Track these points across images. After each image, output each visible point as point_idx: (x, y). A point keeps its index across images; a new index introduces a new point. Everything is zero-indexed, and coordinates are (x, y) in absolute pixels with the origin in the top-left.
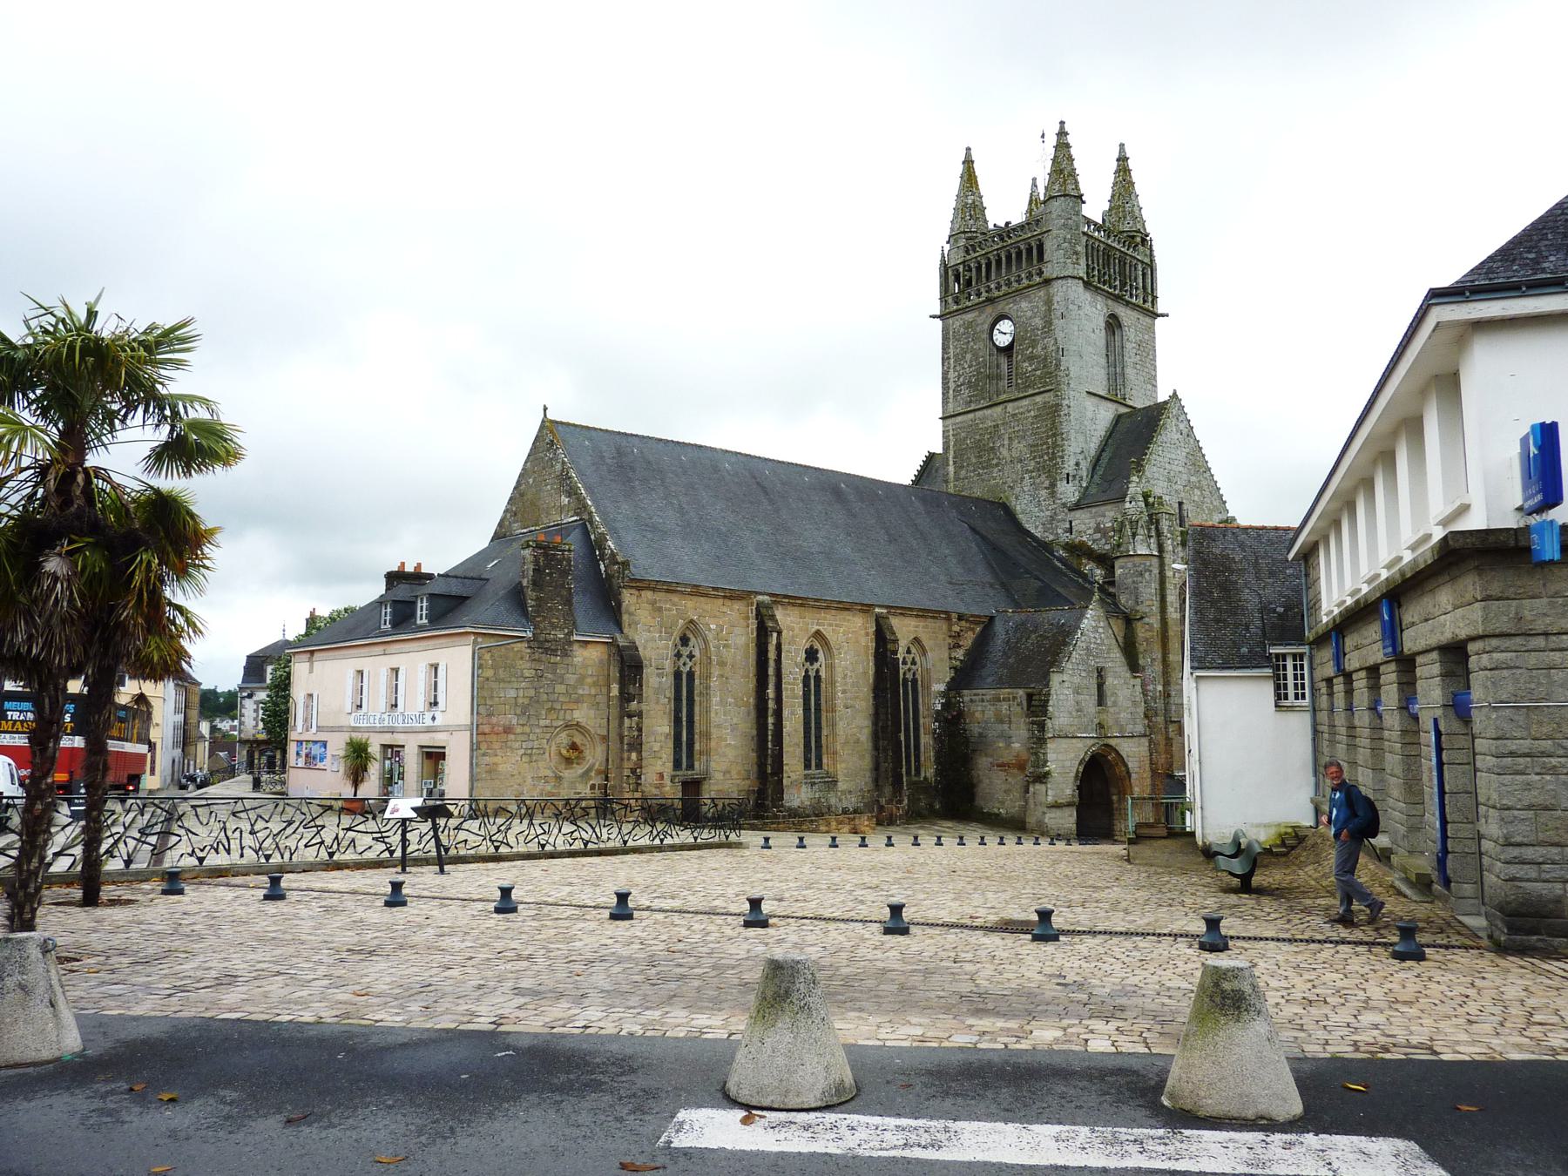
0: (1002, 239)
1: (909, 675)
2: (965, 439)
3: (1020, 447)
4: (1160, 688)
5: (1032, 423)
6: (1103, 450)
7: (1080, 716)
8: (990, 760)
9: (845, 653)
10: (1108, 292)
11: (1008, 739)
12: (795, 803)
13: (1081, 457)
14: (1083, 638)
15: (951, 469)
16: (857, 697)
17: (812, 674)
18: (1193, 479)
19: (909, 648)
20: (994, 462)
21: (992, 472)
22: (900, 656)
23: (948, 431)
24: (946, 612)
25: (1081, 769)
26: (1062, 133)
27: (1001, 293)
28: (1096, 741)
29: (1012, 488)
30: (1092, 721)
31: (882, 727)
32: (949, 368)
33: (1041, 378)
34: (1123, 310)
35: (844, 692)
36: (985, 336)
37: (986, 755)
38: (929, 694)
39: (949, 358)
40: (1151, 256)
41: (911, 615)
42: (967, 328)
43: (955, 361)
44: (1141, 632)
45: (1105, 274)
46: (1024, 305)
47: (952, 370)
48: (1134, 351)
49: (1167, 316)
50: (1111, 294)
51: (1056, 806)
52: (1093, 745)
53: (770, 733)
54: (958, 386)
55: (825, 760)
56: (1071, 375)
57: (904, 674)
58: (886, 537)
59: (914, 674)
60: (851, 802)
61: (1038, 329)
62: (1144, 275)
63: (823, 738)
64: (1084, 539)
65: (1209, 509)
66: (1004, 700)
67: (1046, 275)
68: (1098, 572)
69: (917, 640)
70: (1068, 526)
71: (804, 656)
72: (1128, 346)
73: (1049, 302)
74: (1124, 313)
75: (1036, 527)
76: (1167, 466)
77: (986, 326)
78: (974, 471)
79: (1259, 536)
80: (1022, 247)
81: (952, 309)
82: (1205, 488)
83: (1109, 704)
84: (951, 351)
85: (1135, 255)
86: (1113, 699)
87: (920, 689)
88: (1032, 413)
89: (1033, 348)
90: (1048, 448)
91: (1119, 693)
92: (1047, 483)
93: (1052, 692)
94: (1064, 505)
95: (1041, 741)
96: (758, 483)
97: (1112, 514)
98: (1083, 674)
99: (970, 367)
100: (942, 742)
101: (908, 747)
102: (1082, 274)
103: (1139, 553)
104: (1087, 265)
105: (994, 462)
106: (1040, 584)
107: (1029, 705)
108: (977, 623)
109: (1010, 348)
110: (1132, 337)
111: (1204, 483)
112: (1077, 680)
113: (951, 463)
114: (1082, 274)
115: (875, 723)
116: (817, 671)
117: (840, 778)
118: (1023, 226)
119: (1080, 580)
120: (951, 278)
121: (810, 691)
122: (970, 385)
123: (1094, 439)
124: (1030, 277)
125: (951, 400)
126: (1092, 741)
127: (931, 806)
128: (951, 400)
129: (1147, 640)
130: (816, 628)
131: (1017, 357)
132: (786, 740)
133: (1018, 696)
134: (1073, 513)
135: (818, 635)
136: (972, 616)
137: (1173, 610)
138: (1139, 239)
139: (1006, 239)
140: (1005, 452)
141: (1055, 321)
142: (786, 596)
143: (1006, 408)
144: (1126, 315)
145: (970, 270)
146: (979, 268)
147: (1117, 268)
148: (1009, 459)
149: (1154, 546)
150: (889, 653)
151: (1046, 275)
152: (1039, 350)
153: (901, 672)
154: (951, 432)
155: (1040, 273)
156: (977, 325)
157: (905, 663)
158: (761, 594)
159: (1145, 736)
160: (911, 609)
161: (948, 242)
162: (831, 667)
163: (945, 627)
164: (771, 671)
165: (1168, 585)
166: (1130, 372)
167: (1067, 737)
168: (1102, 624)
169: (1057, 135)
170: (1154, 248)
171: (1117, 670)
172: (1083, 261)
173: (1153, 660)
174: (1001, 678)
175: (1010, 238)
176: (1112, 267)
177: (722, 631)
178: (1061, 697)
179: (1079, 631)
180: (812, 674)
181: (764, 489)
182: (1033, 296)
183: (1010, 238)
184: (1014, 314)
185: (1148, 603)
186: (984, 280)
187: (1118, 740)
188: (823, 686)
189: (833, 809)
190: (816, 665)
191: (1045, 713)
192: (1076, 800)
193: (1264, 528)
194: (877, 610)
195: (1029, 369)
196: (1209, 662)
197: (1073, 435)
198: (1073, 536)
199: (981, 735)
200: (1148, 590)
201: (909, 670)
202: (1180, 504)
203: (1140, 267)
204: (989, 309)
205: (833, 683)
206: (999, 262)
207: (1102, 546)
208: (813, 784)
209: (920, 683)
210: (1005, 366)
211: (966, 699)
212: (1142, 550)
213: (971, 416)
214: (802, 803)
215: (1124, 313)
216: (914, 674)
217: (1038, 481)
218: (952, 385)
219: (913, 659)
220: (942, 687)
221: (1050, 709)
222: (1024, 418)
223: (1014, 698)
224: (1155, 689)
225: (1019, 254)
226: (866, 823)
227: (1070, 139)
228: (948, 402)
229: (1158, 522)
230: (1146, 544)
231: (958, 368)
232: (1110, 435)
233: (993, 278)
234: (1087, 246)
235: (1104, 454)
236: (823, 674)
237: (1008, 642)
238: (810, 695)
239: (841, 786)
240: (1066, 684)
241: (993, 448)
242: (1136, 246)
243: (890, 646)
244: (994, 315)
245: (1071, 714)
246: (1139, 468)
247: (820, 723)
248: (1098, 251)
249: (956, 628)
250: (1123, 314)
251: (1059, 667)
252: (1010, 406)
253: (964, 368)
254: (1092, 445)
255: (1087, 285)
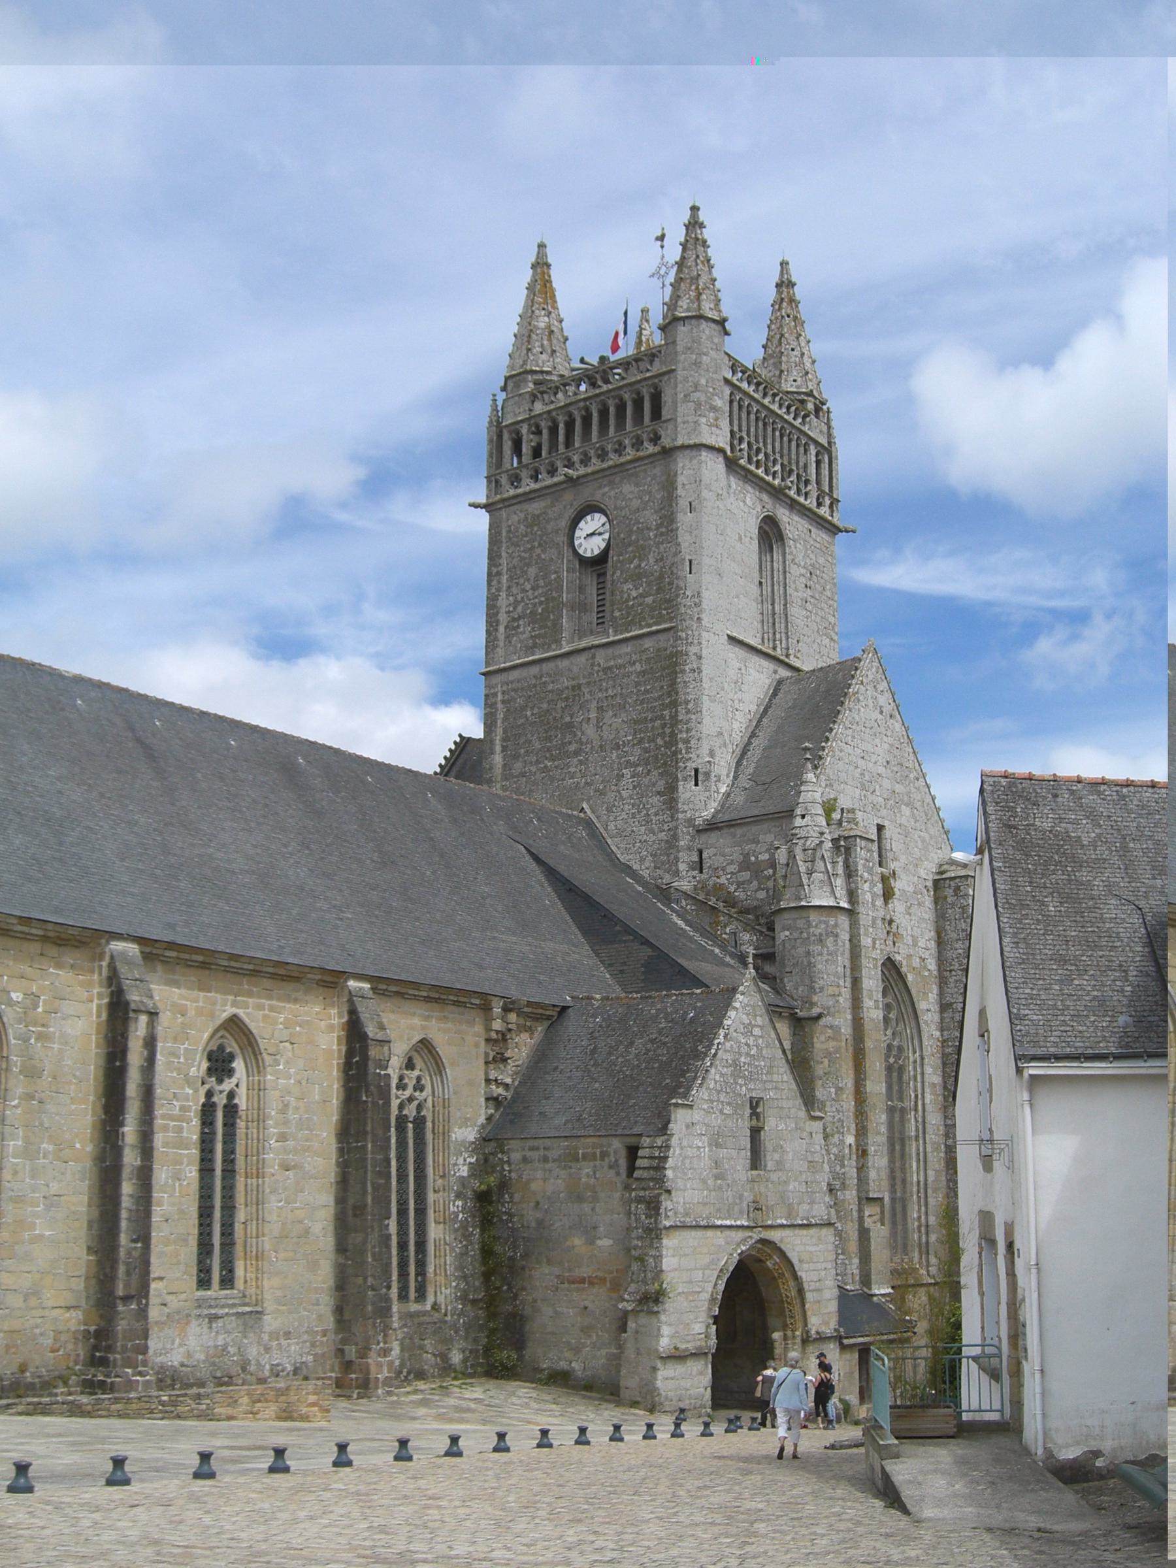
0: (593, 384)
1: (410, 1111)
2: (523, 708)
3: (617, 724)
4: (850, 1139)
5: (638, 684)
6: (753, 735)
7: (720, 1188)
8: (557, 1270)
9: (287, 1062)
10: (762, 479)
11: (591, 1233)
12: (175, 1358)
13: (719, 742)
14: (728, 1045)
15: (498, 759)
16: (308, 1149)
17: (220, 1100)
18: (899, 788)
19: (410, 1059)
20: (572, 747)
21: (568, 766)
22: (394, 1071)
23: (495, 695)
24: (483, 996)
25: (722, 1286)
26: (694, 224)
27: (590, 470)
28: (748, 1233)
29: (602, 793)
30: (741, 1197)
31: (355, 1207)
32: (499, 590)
33: (653, 609)
34: (787, 513)
35: (282, 1138)
36: (562, 539)
37: (549, 1262)
38: (446, 1147)
39: (499, 574)
40: (830, 435)
41: (415, 998)
42: (530, 526)
43: (511, 579)
44: (821, 1042)
45: (758, 451)
46: (628, 488)
47: (503, 594)
48: (803, 580)
49: (854, 532)
50: (768, 483)
51: (678, 1357)
52: (744, 1240)
53: (124, 1214)
54: (514, 620)
55: (239, 1272)
56: (704, 605)
57: (401, 1106)
58: (376, 856)
59: (420, 1107)
60: (291, 1353)
61: (649, 529)
62: (818, 463)
63: (238, 1228)
64: (723, 880)
65: (923, 841)
66: (585, 1157)
67: (666, 442)
68: (746, 937)
69: (425, 1045)
70: (696, 858)
71: (205, 1065)
72: (794, 571)
73: (669, 485)
74: (784, 515)
75: (642, 860)
76: (861, 763)
77: (564, 523)
78: (538, 762)
79: (1123, 797)
80: (626, 397)
81: (506, 495)
82: (918, 805)
83: (770, 1165)
84: (504, 561)
85: (806, 428)
86: (776, 1156)
87: (429, 1136)
88: (638, 667)
89: (641, 560)
90: (664, 726)
91: (788, 1147)
92: (661, 785)
93: (674, 1141)
94: (690, 822)
95: (654, 1234)
96: (138, 740)
97: (769, 838)
98: (728, 1110)
99: (534, 589)
100: (467, 1236)
101: (403, 1246)
102: (723, 441)
103: (816, 902)
104: (732, 432)
105: (572, 747)
106: (648, 951)
107: (631, 1169)
108: (538, 1018)
109: (602, 558)
110: (800, 559)
111: (917, 796)
112: (716, 1121)
113: (498, 748)
114: (723, 441)
115: (341, 1201)
116: (231, 1095)
117: (269, 1306)
118: (628, 363)
119: (717, 951)
120: (508, 446)
121: (213, 1133)
122: (533, 618)
123: (738, 715)
124: (638, 443)
125: (501, 644)
126: (741, 1234)
127: (444, 1357)
128: (501, 644)
129: (829, 1055)
130: (230, 1011)
131: (613, 573)
132: (157, 1235)
133: (611, 1150)
134: (704, 837)
135: (234, 1025)
136: (529, 1004)
137: (871, 1003)
138: (810, 406)
139: (600, 383)
140: (590, 731)
141: (680, 516)
142: (171, 945)
143: (593, 657)
144: (792, 524)
145: (539, 432)
146: (554, 430)
147: (777, 444)
148: (597, 743)
149: (841, 892)
150: (371, 1066)
151: (666, 442)
152: (650, 563)
153: (395, 1103)
154: (500, 695)
155: (656, 439)
156: (548, 521)
157: (401, 1086)
158: (119, 937)
159: (830, 1224)
160: (416, 985)
161: (504, 389)
162: (258, 1090)
163: (479, 1028)
164: (132, 1088)
165: (864, 961)
166: (795, 611)
167: (698, 1227)
168: (759, 1021)
169: (687, 227)
170: (833, 424)
171: (785, 1104)
172: (725, 424)
173: (839, 1090)
174: (579, 1119)
175: (607, 382)
176: (769, 441)
177: (36, 1006)
178: (690, 1152)
179: (722, 1032)
180: (220, 1100)
181: (150, 753)
182: (642, 475)
183: (607, 382)
184: (609, 503)
185: (831, 991)
186: (561, 448)
187: (787, 1232)
188: (241, 1124)
189: (252, 1368)
190: (228, 1085)
191: (660, 1180)
192: (713, 1341)
193: (1128, 784)
194: (352, 983)
195: (634, 594)
196: (1055, 1045)
197: (706, 703)
198: (704, 876)
199: (540, 1223)
200: (831, 968)
201: (411, 1099)
202: (880, 828)
203: (813, 450)
204: (568, 496)
205: (260, 1119)
206: (587, 421)
207: (751, 894)
208: (213, 1318)
209: (429, 1124)
210: (592, 591)
211: (516, 1156)
212: (821, 899)
213: (534, 670)
214: (189, 1355)
215: (784, 515)
216: (420, 1107)
217: (646, 781)
218: (503, 618)
219: (419, 1079)
220: (470, 1134)
221: (669, 1173)
222: (624, 676)
223: (604, 1155)
224: (842, 1142)
225: (621, 408)
226: (312, 1398)
227: (707, 234)
228: (495, 647)
229: (848, 850)
230: (827, 889)
231: (514, 590)
232: (765, 711)
233: (577, 445)
234: (731, 402)
235: (755, 742)
236: (241, 1101)
237: (593, 1052)
238: (212, 1141)
239: (270, 1322)
240: (699, 1129)
241: (570, 725)
242: (804, 417)
243: (373, 1052)
244: (576, 504)
245: (704, 1182)
246: (817, 761)
247: (232, 1197)
248: (749, 413)
249: (497, 1025)
250: (785, 519)
251: (685, 1095)
252: (601, 657)
253: (524, 591)
254: (736, 725)
255: (731, 464)
